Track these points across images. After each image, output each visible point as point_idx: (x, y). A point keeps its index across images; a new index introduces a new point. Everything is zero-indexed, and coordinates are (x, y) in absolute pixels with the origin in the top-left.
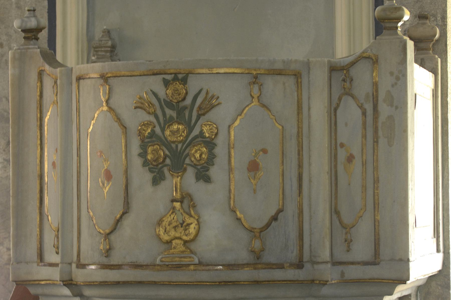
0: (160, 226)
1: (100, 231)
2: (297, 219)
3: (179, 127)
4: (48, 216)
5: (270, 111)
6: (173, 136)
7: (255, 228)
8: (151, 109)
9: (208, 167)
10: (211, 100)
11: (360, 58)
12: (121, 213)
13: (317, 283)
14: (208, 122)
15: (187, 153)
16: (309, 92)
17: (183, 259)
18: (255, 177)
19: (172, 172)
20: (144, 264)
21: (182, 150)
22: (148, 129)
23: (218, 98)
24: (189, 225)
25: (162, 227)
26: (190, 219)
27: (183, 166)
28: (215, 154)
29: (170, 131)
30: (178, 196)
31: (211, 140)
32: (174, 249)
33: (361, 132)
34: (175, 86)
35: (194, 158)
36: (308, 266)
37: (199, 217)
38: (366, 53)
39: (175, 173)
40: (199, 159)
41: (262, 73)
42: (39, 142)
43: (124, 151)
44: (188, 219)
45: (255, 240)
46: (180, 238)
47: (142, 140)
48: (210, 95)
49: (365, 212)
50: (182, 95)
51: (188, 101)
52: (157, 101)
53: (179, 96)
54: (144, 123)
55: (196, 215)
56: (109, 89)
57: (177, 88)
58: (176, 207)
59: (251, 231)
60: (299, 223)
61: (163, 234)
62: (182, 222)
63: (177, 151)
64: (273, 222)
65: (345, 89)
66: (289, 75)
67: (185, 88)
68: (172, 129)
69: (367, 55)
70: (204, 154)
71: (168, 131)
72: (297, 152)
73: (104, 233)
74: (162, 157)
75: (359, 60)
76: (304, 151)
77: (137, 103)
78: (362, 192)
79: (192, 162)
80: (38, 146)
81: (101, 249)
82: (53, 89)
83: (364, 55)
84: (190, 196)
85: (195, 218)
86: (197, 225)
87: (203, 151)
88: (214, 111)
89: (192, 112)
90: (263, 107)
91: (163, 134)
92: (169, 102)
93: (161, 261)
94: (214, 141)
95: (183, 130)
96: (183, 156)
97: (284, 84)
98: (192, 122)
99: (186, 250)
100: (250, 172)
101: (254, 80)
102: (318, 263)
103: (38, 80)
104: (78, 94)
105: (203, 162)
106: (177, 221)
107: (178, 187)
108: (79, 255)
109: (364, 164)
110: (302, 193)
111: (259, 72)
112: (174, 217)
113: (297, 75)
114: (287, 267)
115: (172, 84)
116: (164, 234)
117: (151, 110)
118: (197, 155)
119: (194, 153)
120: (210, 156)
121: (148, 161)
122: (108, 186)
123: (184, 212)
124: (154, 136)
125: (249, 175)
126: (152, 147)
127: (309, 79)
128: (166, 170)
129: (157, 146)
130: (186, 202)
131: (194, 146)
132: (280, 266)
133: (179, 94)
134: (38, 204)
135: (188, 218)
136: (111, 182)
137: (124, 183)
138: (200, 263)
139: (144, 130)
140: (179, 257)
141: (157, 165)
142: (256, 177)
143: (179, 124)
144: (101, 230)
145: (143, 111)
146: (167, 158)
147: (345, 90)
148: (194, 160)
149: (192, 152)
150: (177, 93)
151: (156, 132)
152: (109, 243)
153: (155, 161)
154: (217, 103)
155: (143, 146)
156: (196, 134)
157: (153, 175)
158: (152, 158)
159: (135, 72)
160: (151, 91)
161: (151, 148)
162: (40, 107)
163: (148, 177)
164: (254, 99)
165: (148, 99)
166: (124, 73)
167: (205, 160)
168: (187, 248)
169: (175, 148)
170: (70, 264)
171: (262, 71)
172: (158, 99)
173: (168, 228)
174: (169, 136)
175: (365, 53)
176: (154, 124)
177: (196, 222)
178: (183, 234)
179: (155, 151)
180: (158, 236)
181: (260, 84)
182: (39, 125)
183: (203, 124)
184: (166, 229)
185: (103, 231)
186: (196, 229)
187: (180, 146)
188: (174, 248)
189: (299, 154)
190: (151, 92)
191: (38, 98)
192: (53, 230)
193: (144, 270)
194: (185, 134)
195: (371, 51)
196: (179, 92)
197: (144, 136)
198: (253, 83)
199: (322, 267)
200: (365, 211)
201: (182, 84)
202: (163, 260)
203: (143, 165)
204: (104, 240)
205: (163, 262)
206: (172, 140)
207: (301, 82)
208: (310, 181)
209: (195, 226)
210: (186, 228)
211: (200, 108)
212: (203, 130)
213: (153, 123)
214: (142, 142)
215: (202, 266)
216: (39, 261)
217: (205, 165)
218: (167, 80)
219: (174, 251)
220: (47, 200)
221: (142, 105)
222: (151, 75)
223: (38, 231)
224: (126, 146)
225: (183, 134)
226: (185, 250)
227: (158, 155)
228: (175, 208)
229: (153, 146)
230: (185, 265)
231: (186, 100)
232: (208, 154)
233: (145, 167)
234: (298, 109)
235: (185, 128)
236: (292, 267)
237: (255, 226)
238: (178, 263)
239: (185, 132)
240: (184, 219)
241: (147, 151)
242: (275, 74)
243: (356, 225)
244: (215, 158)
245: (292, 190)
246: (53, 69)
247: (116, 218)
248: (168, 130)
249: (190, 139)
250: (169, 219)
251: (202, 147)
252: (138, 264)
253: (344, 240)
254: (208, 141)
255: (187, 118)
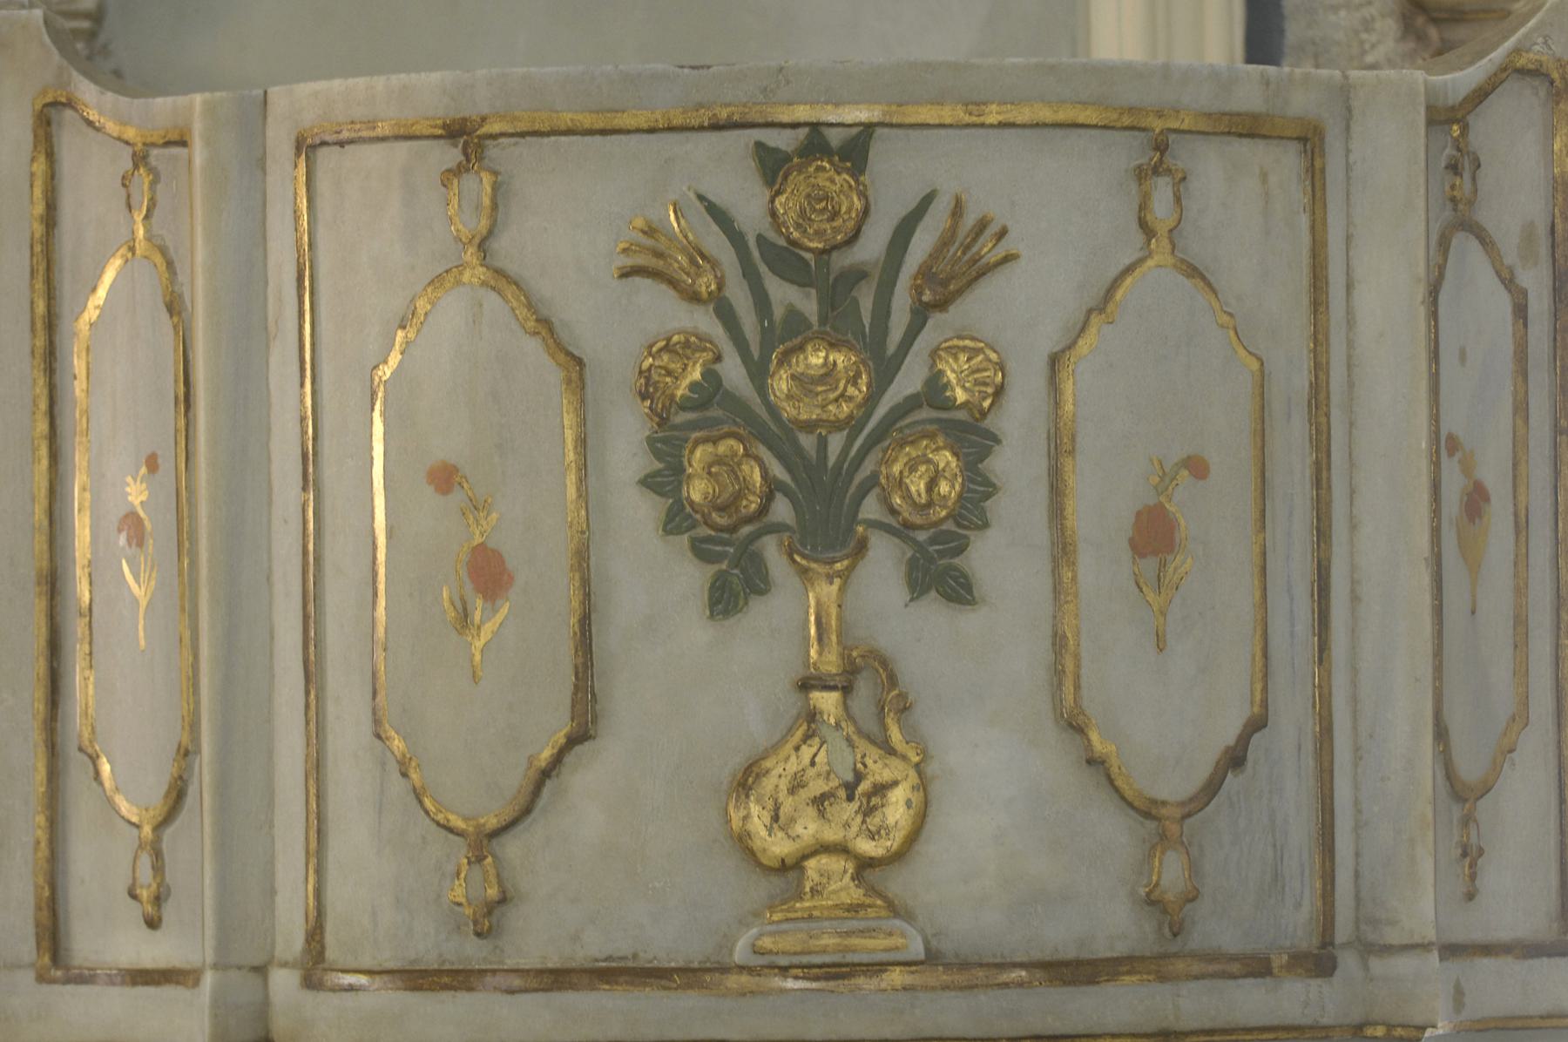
0: (752, 798)
1: (448, 820)
2: (1311, 763)
3: (831, 358)
4: (94, 759)
5: (1214, 292)
6: (806, 400)
7: (1164, 803)
8: (703, 281)
9: (966, 537)
10: (975, 240)
11: (1504, 75)
12: (561, 738)
13: (1376, 1037)
14: (960, 338)
15: (868, 473)
16: (1348, 215)
17: (855, 941)
18: (1159, 581)
19: (804, 556)
20: (673, 965)
21: (849, 459)
22: (686, 365)
23: (1002, 234)
24: (881, 789)
25: (758, 801)
26: (886, 765)
27: (850, 530)
28: (995, 480)
29: (793, 377)
30: (830, 663)
31: (978, 416)
32: (813, 896)
33: (1512, 388)
34: (812, 180)
35: (903, 498)
36: (1348, 962)
37: (925, 754)
38: (1527, 52)
39: (816, 561)
40: (923, 501)
41: (1185, 126)
42: (42, 426)
43: (573, 464)
44: (880, 764)
45: (1163, 853)
46: (841, 849)
47: (661, 417)
48: (969, 220)
49: (1523, 729)
50: (844, 221)
51: (872, 247)
52: (728, 244)
53: (835, 224)
54: (669, 339)
55: (912, 748)
56: (496, 187)
57: (824, 186)
58: (821, 713)
59: (1147, 815)
60: (1321, 777)
61: (763, 833)
62: (850, 777)
63: (825, 464)
64: (1229, 775)
65: (1456, 205)
66: (1281, 138)
67: (861, 188)
68: (801, 369)
69: (1530, 61)
70: (946, 478)
71: (781, 378)
72: (1308, 473)
73: (471, 829)
74: (754, 493)
75: (1502, 82)
76: (1333, 471)
77: (635, 251)
78: (1516, 646)
79: (893, 511)
80: (36, 442)
81: (458, 900)
82: (123, 191)
83: (1521, 62)
84: (884, 668)
85: (910, 760)
86: (918, 790)
87: (942, 465)
88: (986, 290)
89: (892, 293)
90: (1188, 276)
91: (762, 390)
92: (786, 248)
93: (757, 951)
94: (988, 423)
95: (852, 374)
96: (852, 489)
97: (1264, 177)
98: (888, 340)
99: (868, 901)
100: (1142, 555)
101: (1155, 159)
102: (1387, 950)
103: (35, 147)
104: (309, 208)
105: (944, 513)
106: (828, 774)
107: (833, 623)
108: (318, 931)
109: (1521, 527)
110: (1330, 649)
111: (1175, 125)
112: (815, 755)
113: (1309, 140)
114: (1282, 967)
115: (800, 172)
116: (770, 831)
117: (706, 284)
118: (917, 485)
119: (901, 472)
120: (971, 486)
121: (688, 509)
122: (489, 619)
123: (859, 732)
124: (718, 397)
125: (1137, 573)
126: (709, 448)
127: (1347, 156)
128: (771, 549)
129: (732, 442)
130: (864, 689)
131: (902, 444)
132: (1258, 967)
133: (835, 215)
134: (41, 707)
135: (877, 757)
136: (508, 604)
137: (575, 604)
138: (932, 958)
139: (669, 373)
140: (839, 934)
141: (733, 529)
142: (1165, 577)
143: (833, 345)
144: (451, 817)
145: (664, 287)
146: (779, 496)
147: (1455, 210)
148: (904, 506)
149: (895, 469)
150: (825, 209)
151: (724, 383)
152: (498, 875)
153: (721, 509)
154: (999, 256)
155: (664, 441)
156: (909, 391)
157: (712, 569)
158: (710, 497)
159: (625, 115)
160: (701, 198)
161: (704, 450)
162: (49, 269)
163: (692, 578)
164: (1154, 240)
165: (686, 237)
166: (572, 120)
167: (950, 503)
168: (872, 890)
169: (813, 454)
170: (261, 970)
171: (1187, 121)
172: (736, 238)
173: (788, 804)
174: (790, 397)
175: (1524, 54)
176: (716, 346)
177: (913, 777)
178: (855, 829)
179: (725, 464)
180: (743, 844)
181: (1180, 175)
182: (42, 351)
183: (944, 345)
184: (777, 808)
185: (466, 819)
186: (914, 805)
187: (836, 442)
188: (814, 892)
189: (1318, 483)
190: (698, 203)
191: (39, 229)
192: (130, 822)
193: (676, 989)
194: (860, 391)
195: (1546, 43)
196: (833, 207)
197: (673, 396)
198: (1150, 172)
199: (1403, 965)
200: (1527, 725)
201: (848, 171)
202: (767, 942)
203: (665, 525)
204: (469, 863)
205: (763, 954)
206: (804, 417)
207: (1323, 170)
208: (1355, 598)
209: (910, 796)
210: (868, 802)
211: (926, 274)
212: (941, 373)
213: (711, 342)
214: (659, 425)
215: (941, 968)
216: (47, 959)
217: (949, 526)
218: (776, 150)
219: (815, 907)
220: (91, 687)
221: (661, 263)
222: (701, 128)
223: (39, 827)
224: (582, 442)
225: (851, 390)
226: (863, 899)
227: (739, 484)
228: (818, 716)
229: (715, 441)
230: (865, 968)
231: (862, 240)
232: (963, 479)
233: (671, 537)
234: (1315, 287)
235: (863, 362)
236: (1299, 971)
237: (1162, 793)
238: (837, 958)
239: (864, 380)
240: (859, 766)
241: (686, 463)
242: (1234, 134)
243: (1494, 785)
244: (994, 495)
245: (1292, 634)
246: (124, 100)
247: (536, 763)
248: (782, 372)
249: (881, 411)
250: (793, 766)
251: (938, 449)
252: (641, 963)
253: (1459, 851)
254: (961, 422)
255: (867, 321)
